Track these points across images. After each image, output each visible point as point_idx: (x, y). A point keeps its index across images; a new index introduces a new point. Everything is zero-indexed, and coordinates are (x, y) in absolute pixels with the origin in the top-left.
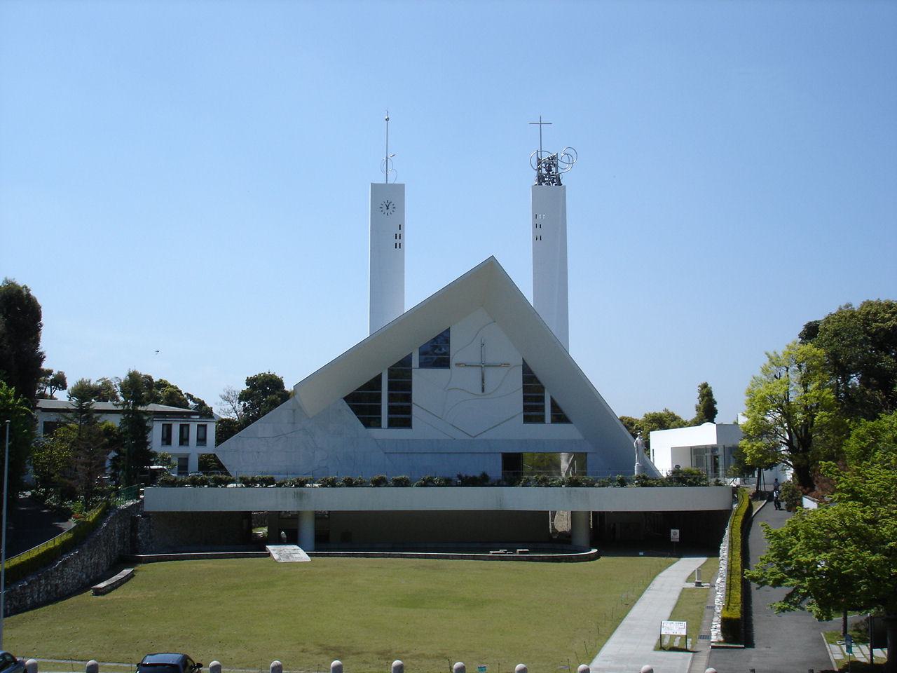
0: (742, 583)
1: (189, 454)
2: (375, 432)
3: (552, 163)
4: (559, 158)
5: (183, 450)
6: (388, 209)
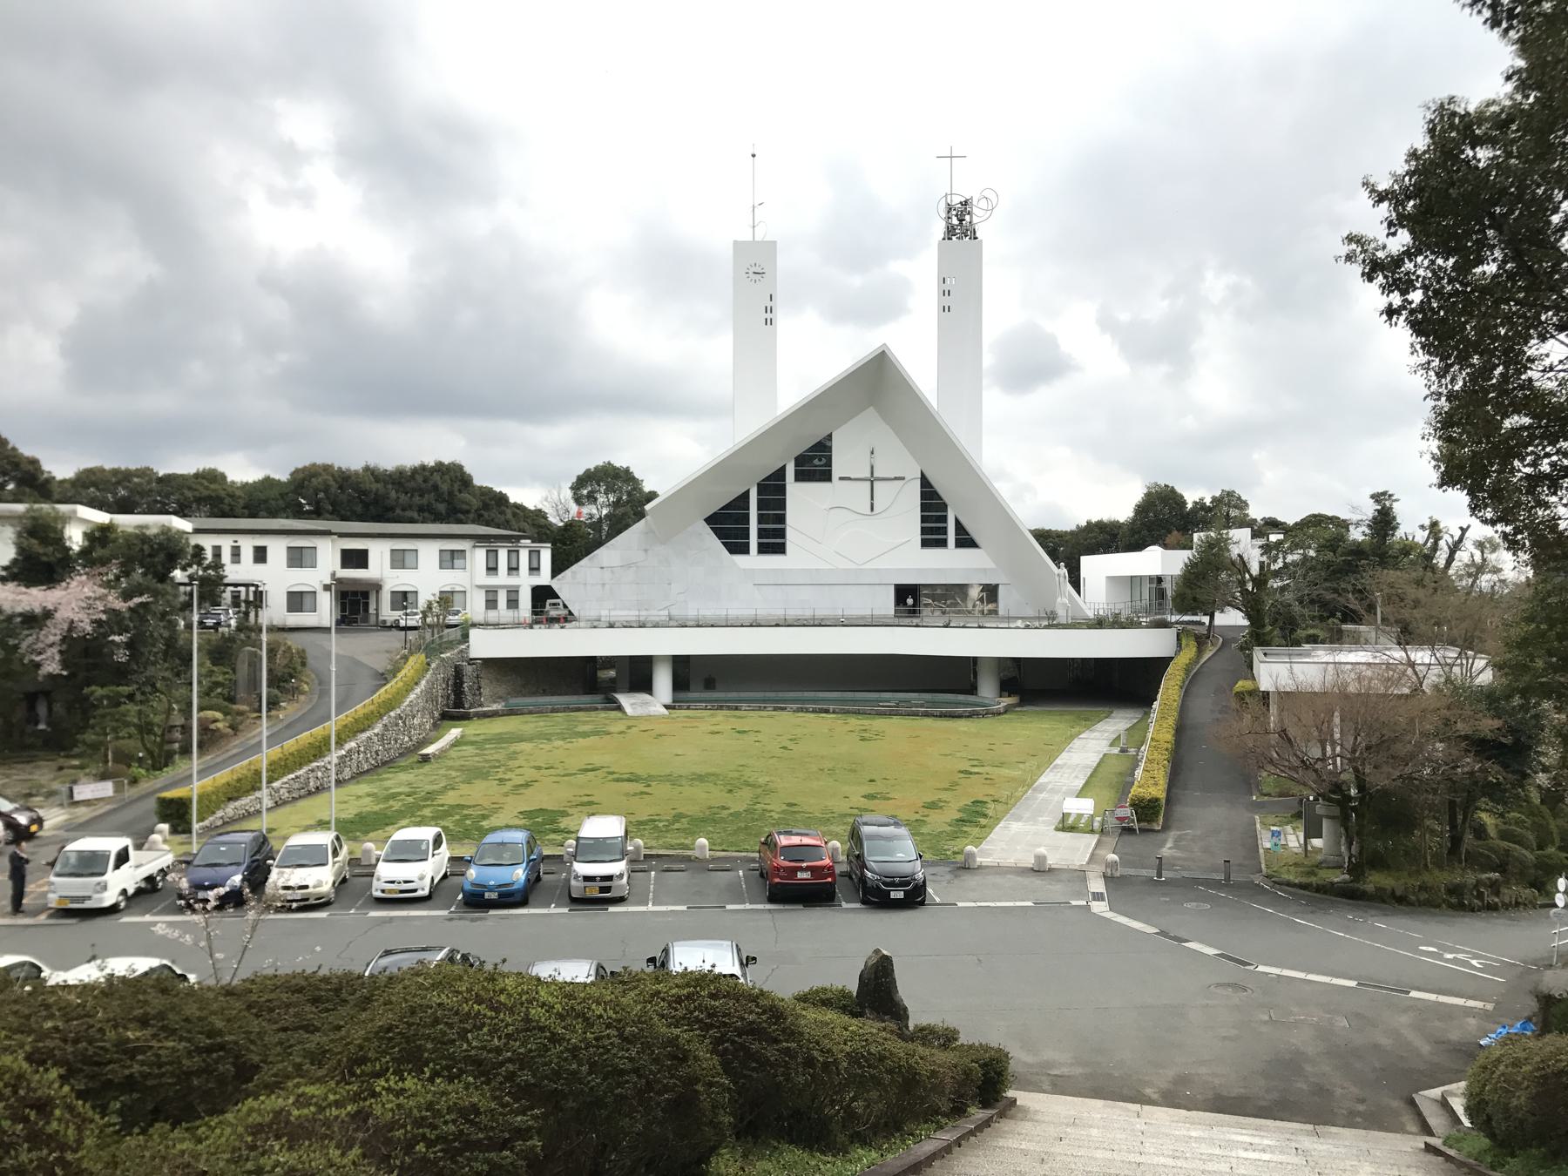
1: (519, 586)
4: (975, 202)
5: (512, 581)
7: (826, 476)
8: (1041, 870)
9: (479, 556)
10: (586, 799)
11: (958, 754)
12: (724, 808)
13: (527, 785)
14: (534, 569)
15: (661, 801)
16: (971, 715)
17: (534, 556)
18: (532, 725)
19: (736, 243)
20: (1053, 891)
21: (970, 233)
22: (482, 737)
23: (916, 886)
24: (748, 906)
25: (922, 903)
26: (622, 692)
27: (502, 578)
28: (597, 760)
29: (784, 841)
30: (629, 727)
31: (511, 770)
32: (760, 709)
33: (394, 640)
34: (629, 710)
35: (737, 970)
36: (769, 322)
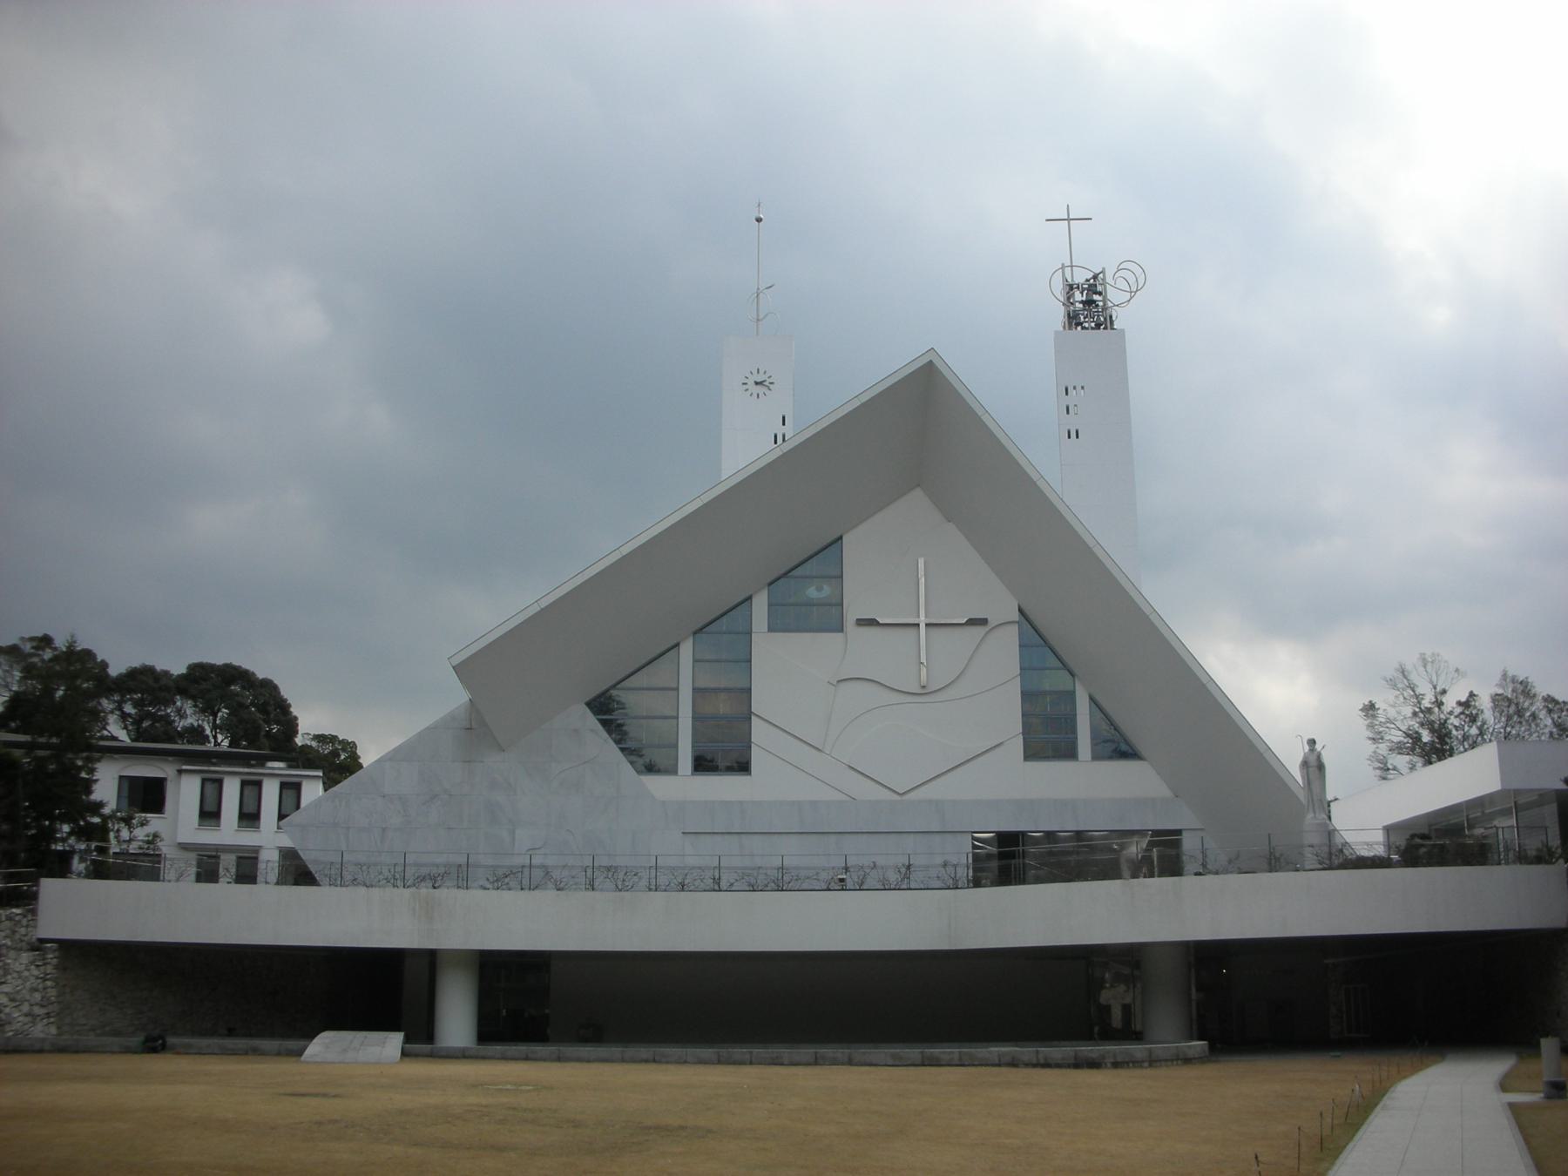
0: (316, 880)
2: (657, 785)
3: (1093, 287)
4: (1109, 280)
5: (247, 838)
6: (757, 383)
21: (1104, 322)
27: (229, 832)
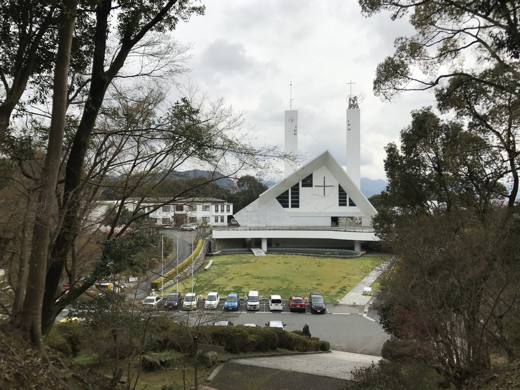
4: (358, 97)
5: (222, 214)
7: (311, 185)
8: (354, 306)
9: (213, 207)
10: (248, 283)
11: (344, 271)
12: (281, 287)
13: (232, 279)
14: (228, 211)
15: (266, 284)
16: (350, 258)
17: (228, 207)
18: (230, 259)
19: (285, 111)
20: (355, 311)
22: (218, 263)
23: (323, 309)
24: (286, 313)
25: (325, 313)
26: (253, 248)
27: (220, 213)
28: (249, 271)
29: (294, 298)
30: (256, 260)
31: (228, 274)
32: (291, 254)
33: (194, 234)
34: (255, 254)
35: (282, 327)
36: (295, 134)
